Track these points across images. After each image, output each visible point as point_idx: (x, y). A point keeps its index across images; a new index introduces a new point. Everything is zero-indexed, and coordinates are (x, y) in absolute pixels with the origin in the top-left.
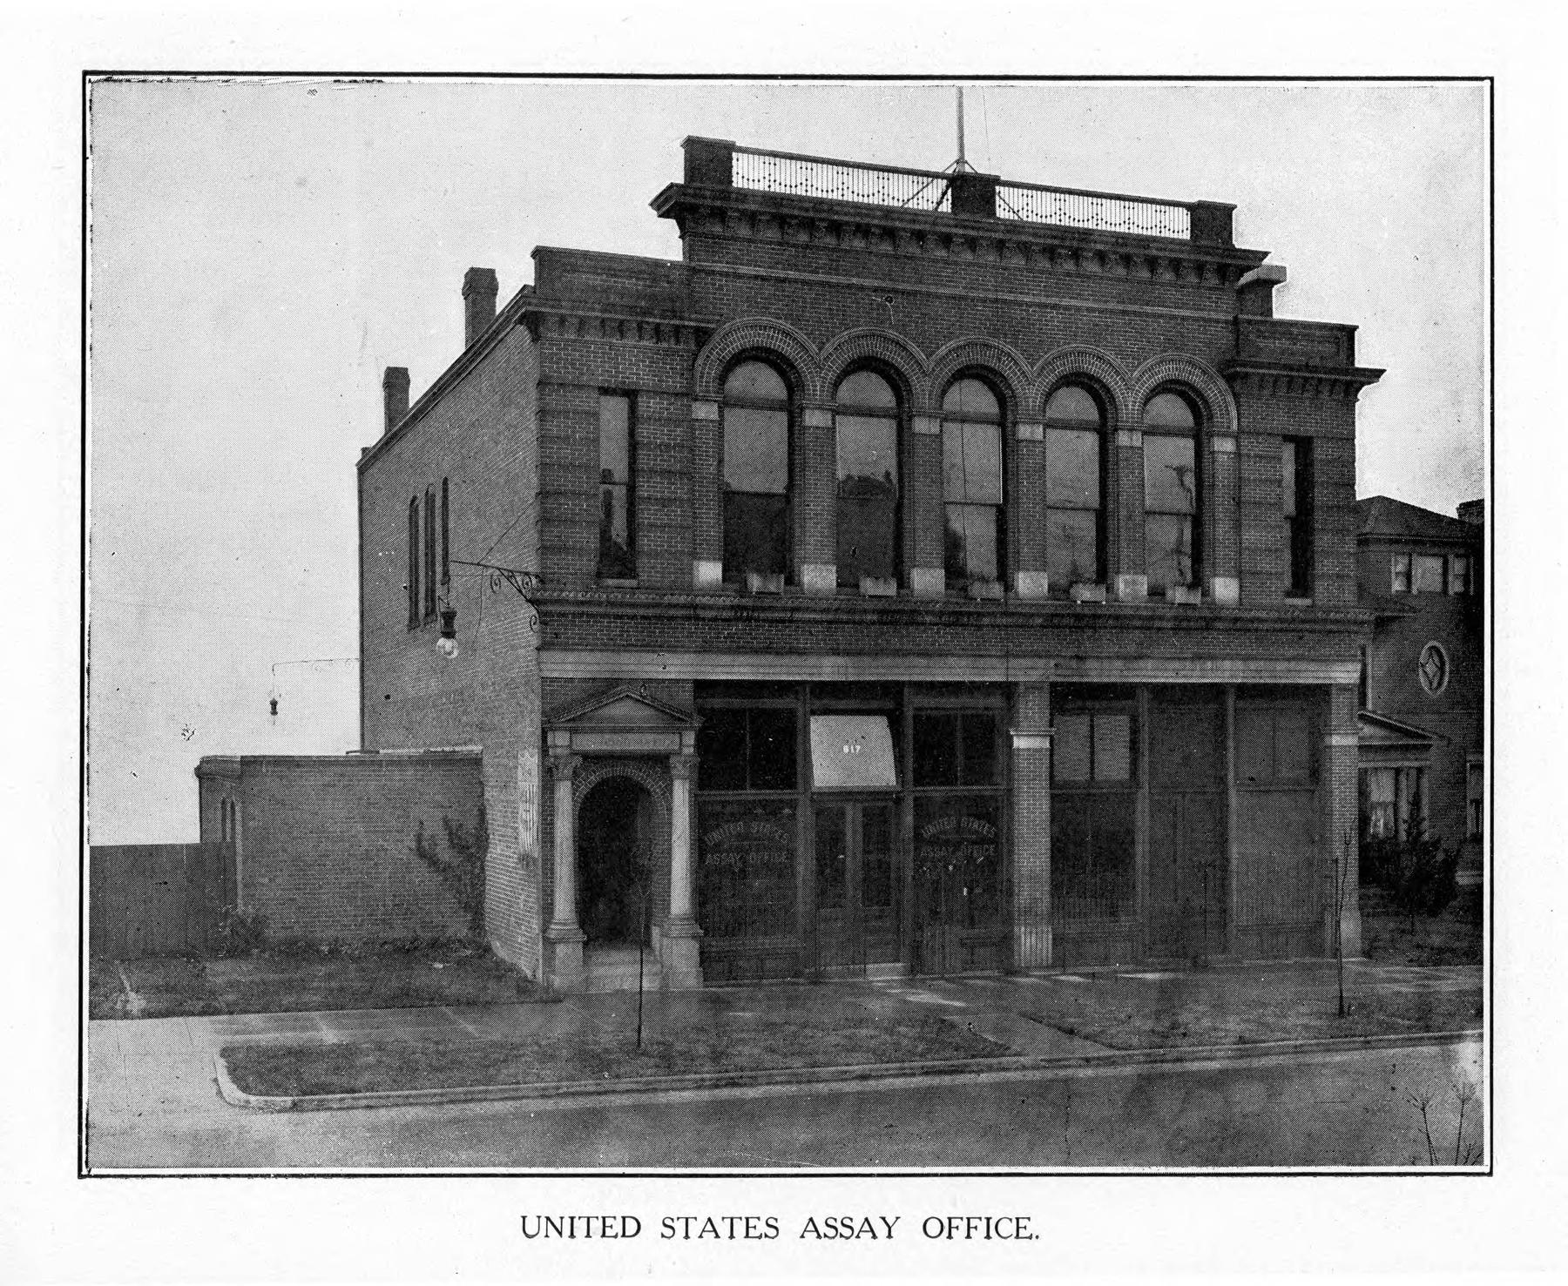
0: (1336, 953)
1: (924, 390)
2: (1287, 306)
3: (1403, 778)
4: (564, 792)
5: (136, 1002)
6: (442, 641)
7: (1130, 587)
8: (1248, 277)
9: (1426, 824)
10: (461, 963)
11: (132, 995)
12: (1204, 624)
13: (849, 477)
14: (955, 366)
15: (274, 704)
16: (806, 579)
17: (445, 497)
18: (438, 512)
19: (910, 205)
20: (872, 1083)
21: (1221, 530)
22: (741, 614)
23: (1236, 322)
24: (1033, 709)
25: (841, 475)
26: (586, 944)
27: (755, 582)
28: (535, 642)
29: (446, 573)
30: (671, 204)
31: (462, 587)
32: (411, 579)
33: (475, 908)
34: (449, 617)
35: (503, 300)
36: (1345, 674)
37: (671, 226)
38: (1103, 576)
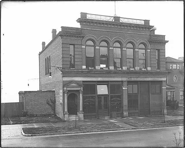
0: (164, 115)
1: (111, 44)
2: (156, 33)
3: (172, 92)
4: (66, 95)
5: (11, 122)
6: (50, 76)
7: (137, 68)
8: (151, 29)
9: (175, 98)
10: (52, 117)
11: (11, 122)
12: (147, 73)
13: (102, 55)
14: (115, 41)
15: (28, 84)
16: (96, 68)
17: (50, 58)
18: (49, 60)
19: (109, 20)
20: (105, 132)
21: (149, 62)
22: (88, 72)
23: (150, 35)
24: (125, 84)
25: (101, 55)
26: (69, 115)
27: (90, 68)
28: (62, 76)
29: (50, 67)
30: (79, 21)
31: (52, 70)
32: (46, 68)
33: (54, 109)
34: (51, 73)
35: (57, 33)
36: (164, 79)
37: (79, 23)
38: (134, 67)
